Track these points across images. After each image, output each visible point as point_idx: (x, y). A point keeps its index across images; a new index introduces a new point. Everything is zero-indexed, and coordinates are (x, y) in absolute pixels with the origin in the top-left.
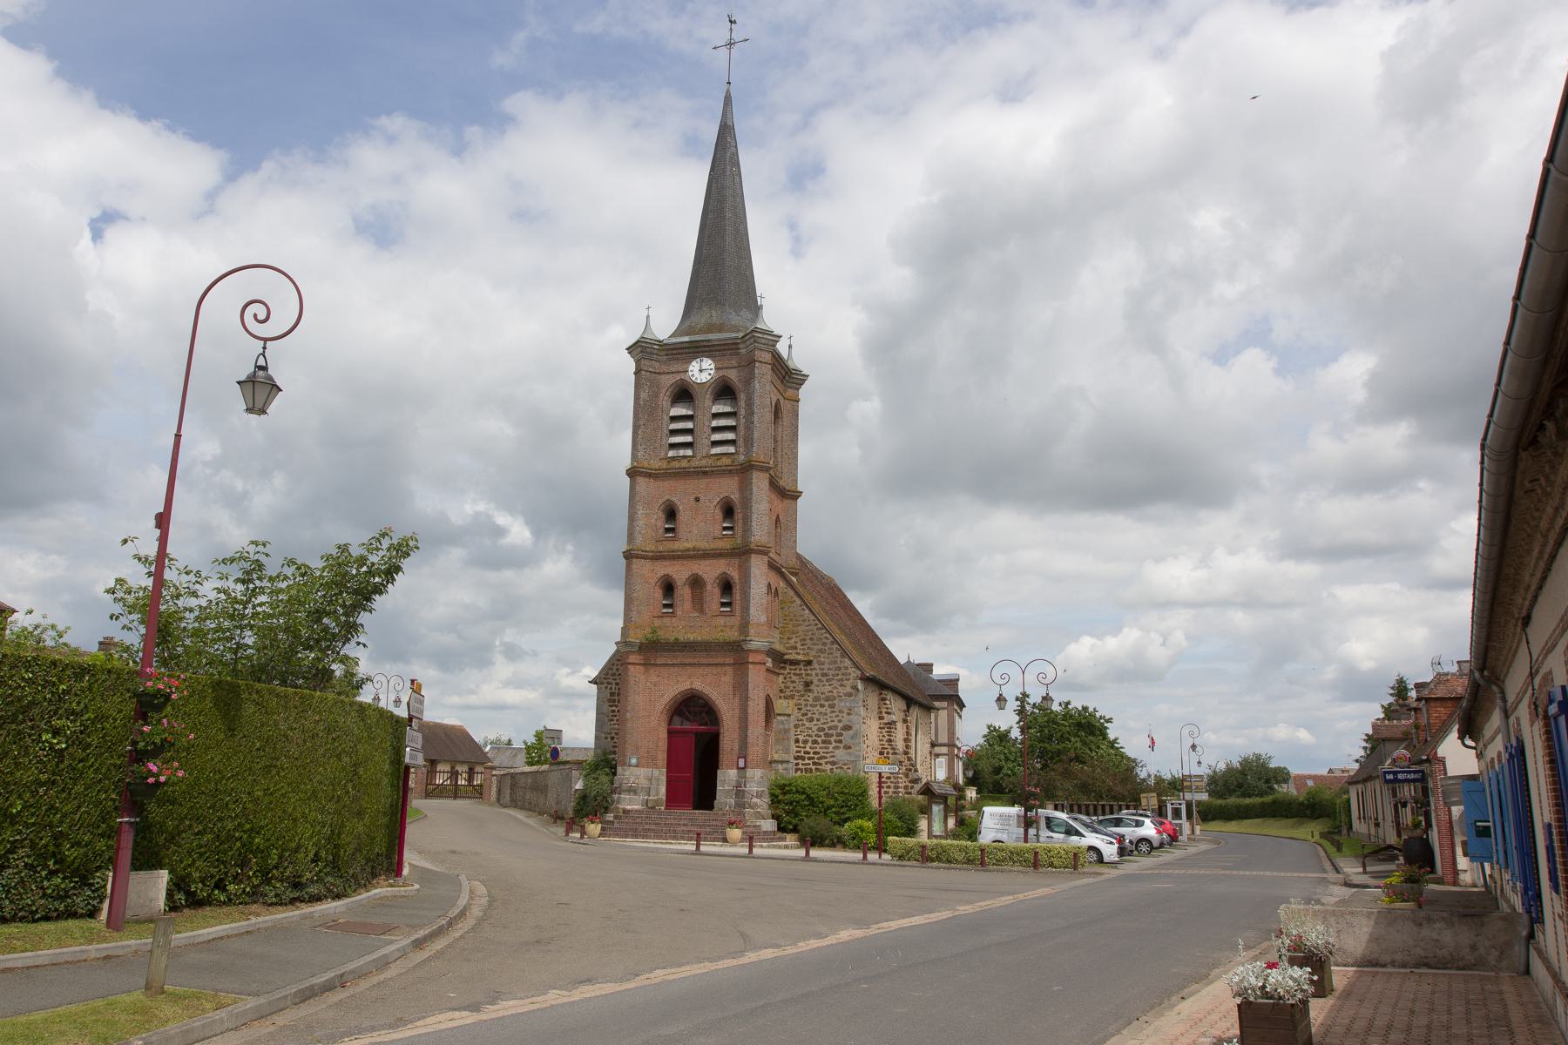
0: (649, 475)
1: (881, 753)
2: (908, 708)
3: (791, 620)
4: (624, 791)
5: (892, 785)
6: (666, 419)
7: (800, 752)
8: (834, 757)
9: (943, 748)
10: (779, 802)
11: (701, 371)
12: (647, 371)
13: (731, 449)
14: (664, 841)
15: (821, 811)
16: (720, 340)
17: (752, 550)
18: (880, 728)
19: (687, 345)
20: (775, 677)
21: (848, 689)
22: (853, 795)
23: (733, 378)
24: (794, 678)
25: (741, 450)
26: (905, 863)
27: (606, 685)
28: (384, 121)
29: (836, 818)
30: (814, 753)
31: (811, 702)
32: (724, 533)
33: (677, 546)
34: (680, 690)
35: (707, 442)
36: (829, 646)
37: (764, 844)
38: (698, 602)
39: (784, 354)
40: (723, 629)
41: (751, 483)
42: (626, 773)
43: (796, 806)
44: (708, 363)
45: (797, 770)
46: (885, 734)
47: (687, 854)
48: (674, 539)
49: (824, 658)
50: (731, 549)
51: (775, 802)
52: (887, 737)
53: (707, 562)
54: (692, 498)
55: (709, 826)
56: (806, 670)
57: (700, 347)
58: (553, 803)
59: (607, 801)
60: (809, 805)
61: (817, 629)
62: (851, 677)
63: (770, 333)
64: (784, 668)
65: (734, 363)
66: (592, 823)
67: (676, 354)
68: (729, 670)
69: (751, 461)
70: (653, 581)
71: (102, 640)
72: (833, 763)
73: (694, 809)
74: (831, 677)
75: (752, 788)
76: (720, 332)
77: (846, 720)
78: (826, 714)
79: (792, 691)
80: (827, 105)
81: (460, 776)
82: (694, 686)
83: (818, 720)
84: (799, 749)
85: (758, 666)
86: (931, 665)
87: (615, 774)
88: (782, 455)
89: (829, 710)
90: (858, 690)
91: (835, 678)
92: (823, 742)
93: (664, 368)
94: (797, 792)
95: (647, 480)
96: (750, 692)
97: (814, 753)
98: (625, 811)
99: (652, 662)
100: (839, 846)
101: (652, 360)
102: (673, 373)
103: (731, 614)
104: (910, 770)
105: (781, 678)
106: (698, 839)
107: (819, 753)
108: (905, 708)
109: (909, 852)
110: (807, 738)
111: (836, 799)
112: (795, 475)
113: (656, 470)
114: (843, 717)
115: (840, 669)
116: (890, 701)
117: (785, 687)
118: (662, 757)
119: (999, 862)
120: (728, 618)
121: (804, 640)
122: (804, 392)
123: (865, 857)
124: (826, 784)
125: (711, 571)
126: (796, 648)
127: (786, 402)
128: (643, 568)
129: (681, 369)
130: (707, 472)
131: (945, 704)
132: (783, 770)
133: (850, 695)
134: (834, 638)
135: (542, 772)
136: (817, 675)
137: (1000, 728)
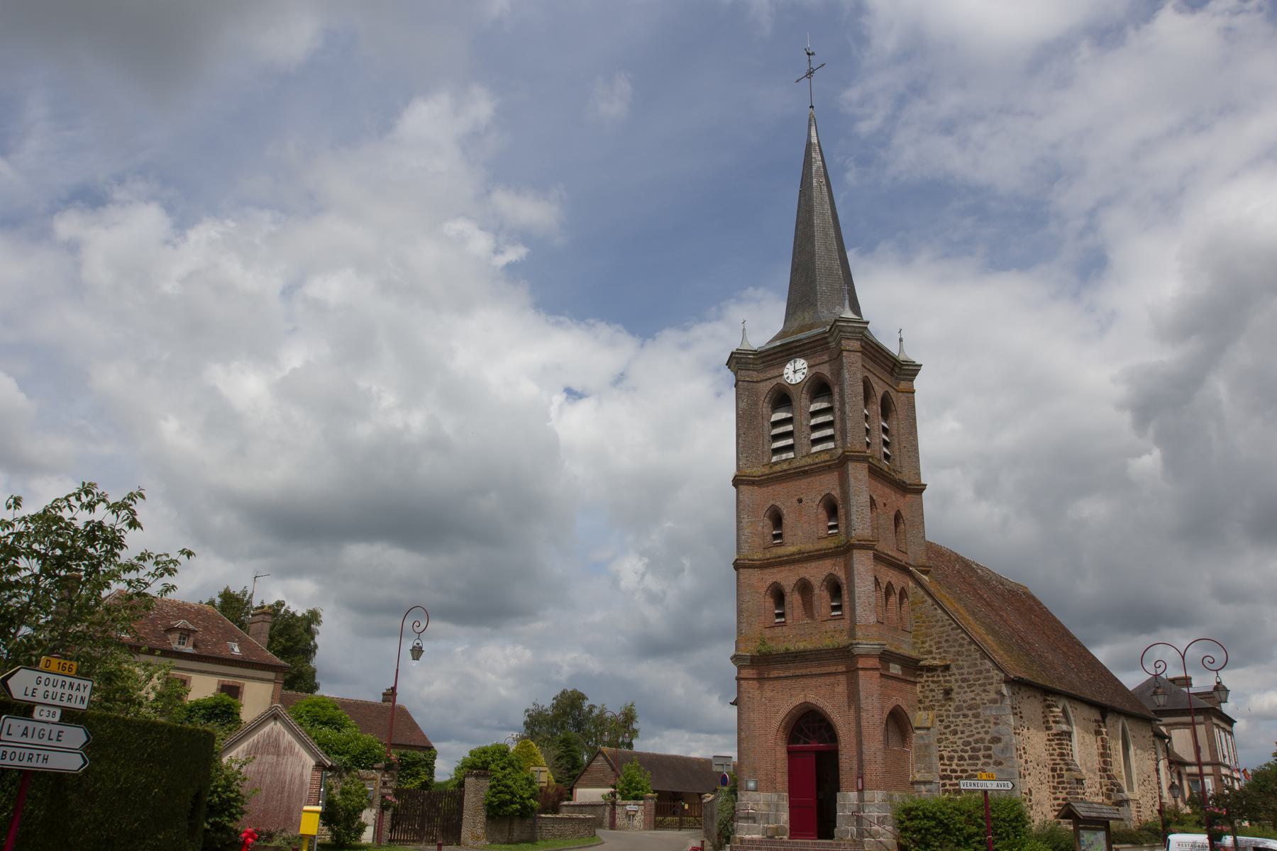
0: (753, 483)
1: (1053, 770)
3: (924, 622)
4: (740, 818)
6: (767, 425)
7: (946, 770)
11: (795, 372)
12: (744, 381)
13: (831, 445)
16: (808, 338)
17: (853, 545)
18: (1049, 740)
19: (780, 349)
21: (993, 695)
22: (1004, 820)
23: (825, 373)
24: (933, 686)
30: (963, 771)
31: (953, 712)
32: (830, 532)
34: (794, 705)
36: (966, 647)
38: (808, 606)
42: (743, 799)
43: (926, 835)
44: (801, 364)
46: (1056, 747)
48: (780, 545)
50: (835, 548)
52: (1058, 751)
53: (813, 564)
54: (795, 500)
56: (943, 676)
57: (792, 348)
61: (952, 629)
62: (994, 681)
65: (826, 358)
67: (771, 360)
68: (842, 679)
70: (763, 591)
71: (385, 691)
73: (820, 838)
74: (972, 682)
75: (872, 813)
77: (993, 730)
78: (970, 725)
83: (962, 732)
84: (944, 767)
85: (871, 672)
88: (900, 449)
89: (974, 720)
90: (1003, 695)
91: (977, 683)
92: (971, 758)
93: (762, 376)
94: (926, 817)
97: (963, 771)
98: (742, 840)
99: (766, 676)
101: (749, 370)
102: (770, 379)
103: (841, 617)
104: (1112, 790)
105: (918, 687)
110: (952, 754)
113: (759, 477)
114: (989, 727)
115: (981, 672)
117: (924, 697)
118: (782, 779)
120: (837, 622)
121: (939, 642)
122: (919, 383)
124: (965, 807)
125: (816, 573)
126: (931, 652)
127: (900, 394)
129: (777, 374)
132: (926, 791)
133: (994, 701)
134: (971, 638)
136: (956, 681)
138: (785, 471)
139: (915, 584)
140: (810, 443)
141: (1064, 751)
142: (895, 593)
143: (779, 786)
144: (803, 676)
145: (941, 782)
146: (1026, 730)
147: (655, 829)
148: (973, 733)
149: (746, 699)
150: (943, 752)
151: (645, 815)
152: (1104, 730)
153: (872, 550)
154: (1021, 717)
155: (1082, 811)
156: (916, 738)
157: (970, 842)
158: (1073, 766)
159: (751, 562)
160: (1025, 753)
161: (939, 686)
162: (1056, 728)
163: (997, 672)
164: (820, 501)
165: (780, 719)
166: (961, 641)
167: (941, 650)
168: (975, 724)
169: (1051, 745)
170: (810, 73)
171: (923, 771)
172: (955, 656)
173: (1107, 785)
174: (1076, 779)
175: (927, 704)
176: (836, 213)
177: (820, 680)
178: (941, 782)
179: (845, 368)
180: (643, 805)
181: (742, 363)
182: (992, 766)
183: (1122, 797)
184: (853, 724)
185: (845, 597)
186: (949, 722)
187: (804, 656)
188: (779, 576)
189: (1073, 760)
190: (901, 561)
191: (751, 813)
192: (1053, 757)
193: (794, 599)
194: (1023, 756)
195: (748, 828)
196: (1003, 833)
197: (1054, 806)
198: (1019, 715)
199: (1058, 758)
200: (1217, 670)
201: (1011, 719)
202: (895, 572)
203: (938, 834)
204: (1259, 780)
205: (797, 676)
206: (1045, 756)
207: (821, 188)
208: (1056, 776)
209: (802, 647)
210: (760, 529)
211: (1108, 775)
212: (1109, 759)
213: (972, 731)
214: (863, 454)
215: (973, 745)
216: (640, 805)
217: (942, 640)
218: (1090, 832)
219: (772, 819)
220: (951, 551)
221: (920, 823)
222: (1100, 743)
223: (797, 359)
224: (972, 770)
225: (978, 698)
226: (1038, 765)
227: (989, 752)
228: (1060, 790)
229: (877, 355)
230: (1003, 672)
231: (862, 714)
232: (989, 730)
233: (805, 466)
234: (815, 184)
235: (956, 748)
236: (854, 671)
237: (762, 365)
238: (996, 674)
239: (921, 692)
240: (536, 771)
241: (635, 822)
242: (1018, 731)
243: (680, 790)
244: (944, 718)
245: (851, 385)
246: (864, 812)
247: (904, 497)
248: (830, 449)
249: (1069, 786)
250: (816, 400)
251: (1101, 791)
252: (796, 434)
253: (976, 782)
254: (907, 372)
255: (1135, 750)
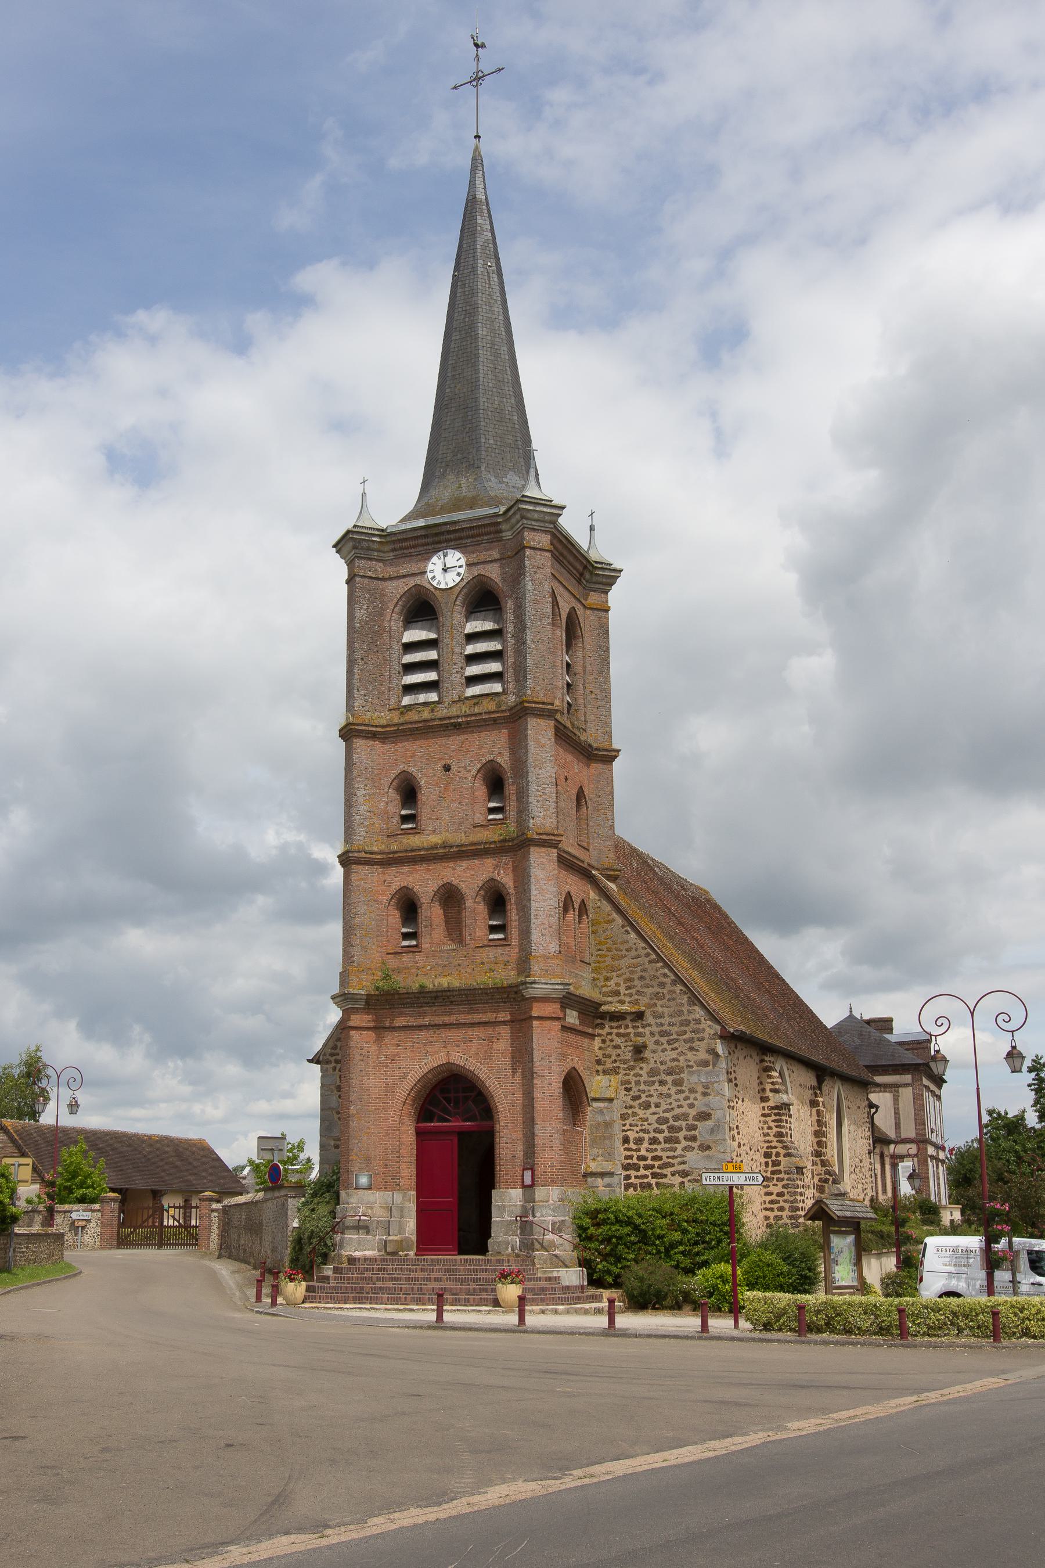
0: (373, 736)
1: (767, 1155)
2: (820, 1081)
3: (609, 950)
4: (348, 1228)
5: (787, 1206)
6: (397, 647)
7: (631, 1157)
8: (684, 1163)
9: (908, 1146)
10: (590, 1238)
11: (445, 570)
12: (363, 577)
13: (497, 687)
14: (401, 1307)
15: (659, 1252)
16: (471, 520)
18: (763, 1115)
19: (423, 532)
20: (586, 1040)
21: (703, 1055)
22: (714, 1224)
24: (618, 1041)
25: (511, 687)
26: (773, 1335)
27: (333, 1064)
28: (141, 316)
29: (686, 1262)
30: (654, 1158)
31: (645, 1077)
32: (491, 817)
33: (415, 841)
34: (430, 1066)
35: (458, 679)
36: (669, 987)
37: (561, 1307)
38: (455, 926)
39: (581, 539)
40: (492, 966)
41: (526, 736)
42: (352, 1200)
44: (455, 558)
45: (627, 1187)
46: (772, 1124)
47: (421, 1327)
48: (414, 832)
49: (662, 1006)
51: (583, 1236)
52: (775, 1129)
53: (465, 864)
54: (439, 766)
55: (474, 1280)
56: (633, 1027)
57: (442, 533)
58: (269, 1251)
59: (326, 1245)
60: (639, 1242)
62: (706, 1035)
63: (548, 503)
64: (601, 1026)
65: (495, 554)
66: (292, 1280)
68: (505, 1031)
69: (522, 702)
72: (684, 1174)
74: (674, 1036)
76: (471, 508)
77: (700, 1104)
78: (669, 1096)
79: (616, 1061)
80: (747, 240)
81: (165, 1213)
82: (451, 1061)
83: (657, 1106)
84: (629, 1153)
85: (548, 1023)
86: (890, 1020)
87: (337, 1200)
88: (585, 695)
89: (674, 1089)
90: (717, 1055)
92: (667, 1140)
93: (391, 571)
94: (618, 1221)
95: (370, 743)
96: (536, 1065)
97: (654, 1158)
98: (352, 1260)
99: (387, 1024)
100: (687, 1308)
102: (404, 576)
103: (505, 943)
104: (826, 1181)
106: (440, 1301)
107: (660, 1158)
108: (815, 1084)
109: (780, 1316)
110: (641, 1134)
111: (685, 1232)
112: (608, 724)
113: (383, 727)
114: (696, 1099)
115: (687, 1023)
116: (781, 1075)
117: (605, 1056)
118: (408, 1171)
119: (933, 1330)
120: (499, 950)
121: (630, 980)
122: (616, 596)
123: (705, 1326)
124: (667, 1208)
126: (617, 993)
127: (588, 612)
128: (369, 878)
129: (415, 570)
130: (460, 724)
131: (907, 1078)
133: (705, 1064)
134: (676, 974)
135: (257, 1201)
136: (652, 1034)
137: (1006, 1113)
138: (425, 721)
139: (599, 895)
140: (464, 681)
141: (783, 1130)
142: (574, 908)
143: (404, 1182)
144: (445, 1025)
145: (625, 1173)
146: (740, 1102)
147: (118, 1248)
148: (672, 1106)
149: (358, 1058)
150: (628, 1133)
151: (103, 1225)
152: (820, 1099)
153: (556, 848)
154: (736, 1085)
155: (835, 1208)
156: (592, 1113)
157: (672, 1252)
158: (792, 1151)
159: (368, 856)
160: (738, 1133)
161: (626, 1041)
162: (774, 1100)
163: (710, 1023)
164: (479, 771)
165: (408, 1087)
166: (662, 979)
167: (633, 991)
168: (676, 1094)
169: (766, 1122)
170: (477, 79)
171: (600, 1158)
172: (651, 999)
173: (821, 1174)
174: (797, 1168)
175: (609, 1065)
176: (509, 320)
177: (470, 1031)
178: (625, 1173)
179: (528, 575)
180: (99, 1211)
181: (362, 548)
182: (696, 1151)
183: (838, 1189)
184: (519, 1095)
185: (513, 914)
186: (639, 1090)
187: (448, 997)
188: (411, 878)
189: (792, 1142)
190: (583, 862)
191: (364, 1220)
192: (768, 1138)
193: (432, 914)
194: (737, 1137)
195: (359, 1242)
196: (712, 1240)
197: (765, 1203)
198: (734, 1082)
199: (775, 1139)
200: (1012, 1032)
201: (726, 1089)
202: (575, 878)
203: (633, 1243)
204: (965, 1162)
205: (436, 1025)
206: (758, 1138)
207: (489, 276)
208: (770, 1164)
209: (446, 985)
210: (382, 805)
211: (822, 1161)
212: (824, 1139)
213: (670, 1104)
214: (549, 707)
215: (671, 1122)
216: (93, 1211)
217: (635, 976)
218: (841, 1235)
219: (394, 1228)
220: (622, 839)
221: (610, 1229)
222: (815, 1118)
223: (449, 551)
224: (668, 1157)
225: (681, 1058)
226: (751, 1150)
227: (693, 1132)
228: (775, 1182)
229: (565, 553)
230: (719, 1023)
231: (535, 1081)
232: (695, 1102)
233: (458, 717)
234: (480, 270)
235: (647, 1127)
236: (525, 1020)
237: (392, 554)
238: (709, 1026)
239: (600, 1048)
240: (13, 1165)
241: (86, 1237)
242: (732, 1104)
243: (127, 1186)
244: (633, 1085)
245: (535, 601)
246: (534, 1216)
247: (588, 766)
248: (497, 694)
249: (786, 1176)
250: (473, 615)
251: (812, 1183)
252: (444, 665)
253: (721, 1175)
254: (600, 579)
255: (849, 1126)
